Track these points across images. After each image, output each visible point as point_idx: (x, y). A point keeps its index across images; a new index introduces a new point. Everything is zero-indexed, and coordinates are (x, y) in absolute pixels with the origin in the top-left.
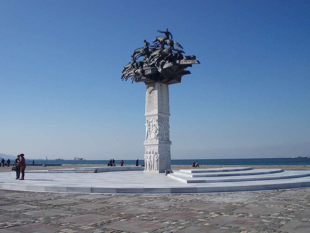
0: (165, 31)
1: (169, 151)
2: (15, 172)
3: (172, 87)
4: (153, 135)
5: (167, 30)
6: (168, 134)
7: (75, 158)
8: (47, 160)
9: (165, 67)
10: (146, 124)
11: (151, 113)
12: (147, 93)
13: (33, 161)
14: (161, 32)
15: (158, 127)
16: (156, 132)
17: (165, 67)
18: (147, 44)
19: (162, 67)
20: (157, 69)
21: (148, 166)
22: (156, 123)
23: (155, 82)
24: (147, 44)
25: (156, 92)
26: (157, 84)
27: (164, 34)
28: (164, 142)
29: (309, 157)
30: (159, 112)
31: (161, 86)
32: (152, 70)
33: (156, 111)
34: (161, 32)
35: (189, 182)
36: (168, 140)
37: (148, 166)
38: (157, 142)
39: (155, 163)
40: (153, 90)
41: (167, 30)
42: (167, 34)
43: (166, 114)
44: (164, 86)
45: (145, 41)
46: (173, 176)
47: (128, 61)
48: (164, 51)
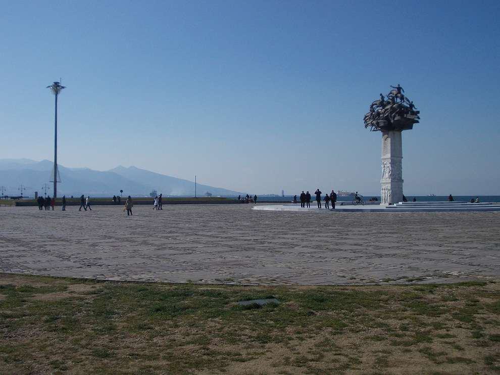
0: (397, 86)
1: (402, 188)
2: (414, 124)
3: (405, 133)
4: (387, 175)
5: (399, 85)
6: (400, 173)
7: (339, 192)
8: (284, 196)
9: (396, 119)
10: (382, 166)
11: (385, 157)
12: (383, 141)
13: (256, 197)
14: (394, 87)
15: (390, 168)
16: (389, 173)
17: (396, 119)
18: (383, 98)
19: (394, 119)
20: (390, 120)
21: (383, 200)
22: (389, 165)
23: (389, 131)
24: (383, 98)
25: (389, 139)
26: (390, 133)
27: (396, 89)
28: (396, 180)
29: (499, 194)
30: (391, 156)
31: (394, 134)
32: (384, 122)
33: (389, 155)
34: (394, 87)
35: (387, 207)
36: (401, 178)
37: (383, 200)
38: (390, 181)
39: (389, 197)
40: (388, 137)
41: (399, 85)
42: (399, 89)
43: (398, 157)
44: (397, 133)
45: (381, 95)
46: (368, 206)
47: (367, 111)
48: (394, 106)
